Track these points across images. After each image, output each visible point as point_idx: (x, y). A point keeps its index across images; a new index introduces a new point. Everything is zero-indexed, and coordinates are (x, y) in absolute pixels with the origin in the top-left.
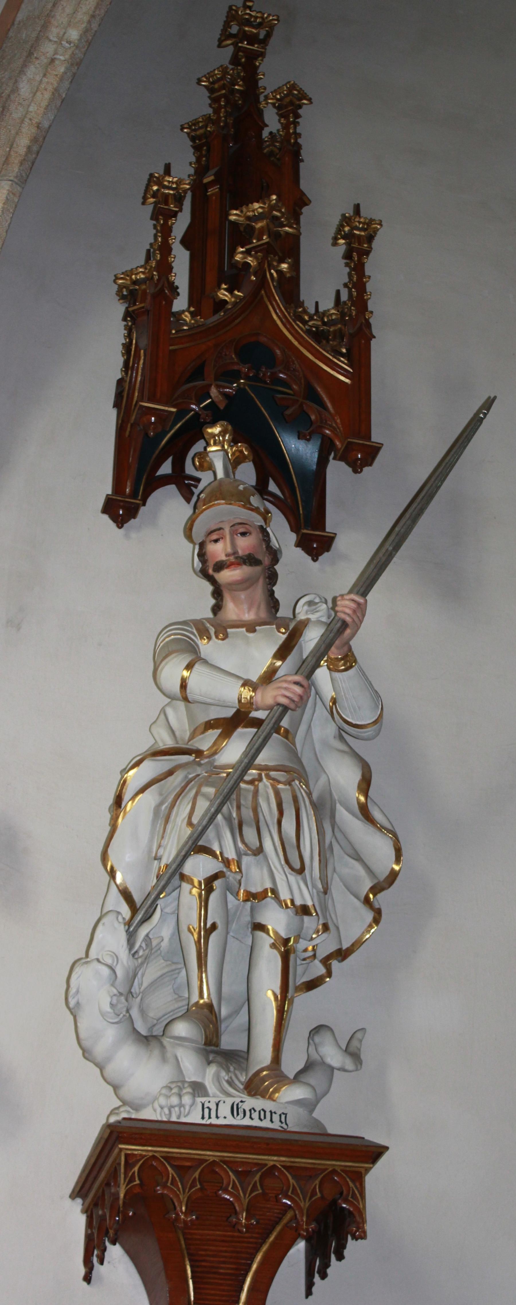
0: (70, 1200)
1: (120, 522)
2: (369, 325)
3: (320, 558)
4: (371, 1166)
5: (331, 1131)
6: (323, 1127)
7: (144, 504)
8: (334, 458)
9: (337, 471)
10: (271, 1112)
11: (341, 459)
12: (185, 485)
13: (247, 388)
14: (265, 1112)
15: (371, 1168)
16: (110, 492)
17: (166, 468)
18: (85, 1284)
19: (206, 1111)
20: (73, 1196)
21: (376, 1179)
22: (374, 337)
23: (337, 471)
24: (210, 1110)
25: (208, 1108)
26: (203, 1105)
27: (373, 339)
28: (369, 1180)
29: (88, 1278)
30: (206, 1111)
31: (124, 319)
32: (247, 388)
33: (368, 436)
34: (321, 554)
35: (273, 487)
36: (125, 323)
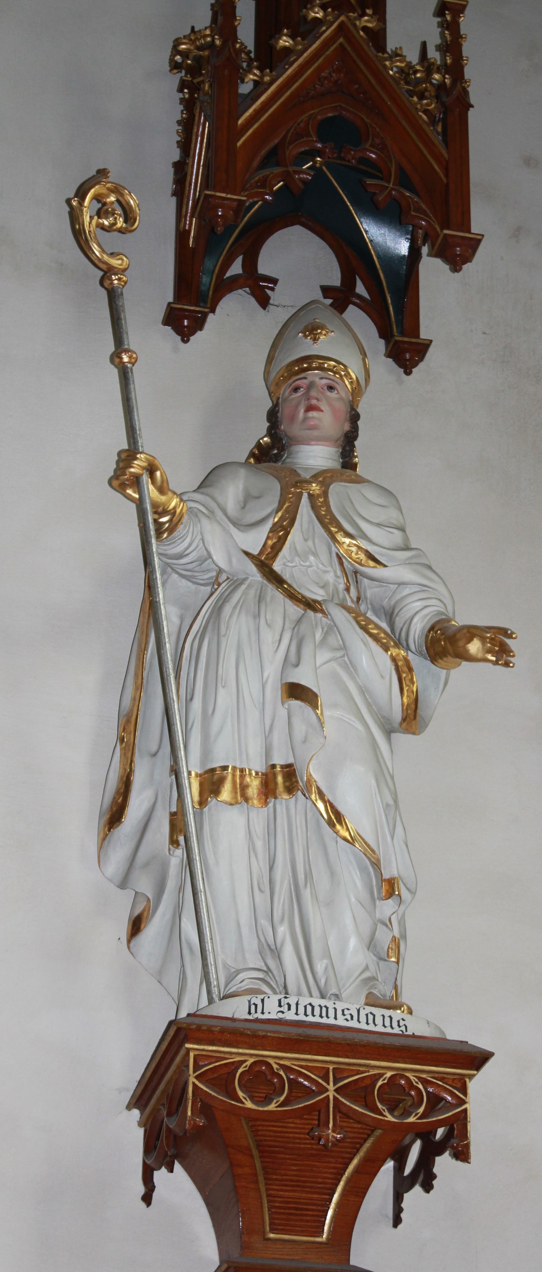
0: (127, 1111)
1: (185, 335)
2: (466, 93)
3: (192, 338)
4: (475, 1072)
5: (450, 1037)
6: (443, 1033)
7: (213, 311)
8: (429, 255)
9: (431, 269)
10: (320, 1006)
11: (436, 255)
12: (261, 289)
13: (324, 168)
14: (313, 1007)
15: (474, 1075)
16: (171, 300)
17: (236, 268)
18: (143, 1205)
19: (253, 1007)
20: (129, 1107)
21: (480, 1087)
22: (472, 107)
23: (431, 269)
24: (256, 1005)
25: (254, 1004)
26: (250, 1002)
27: (471, 109)
28: (472, 1086)
29: (147, 1199)
30: (253, 1007)
31: (180, 90)
32: (324, 168)
33: (465, 225)
34: (193, 333)
35: (360, 289)
36: (181, 95)
